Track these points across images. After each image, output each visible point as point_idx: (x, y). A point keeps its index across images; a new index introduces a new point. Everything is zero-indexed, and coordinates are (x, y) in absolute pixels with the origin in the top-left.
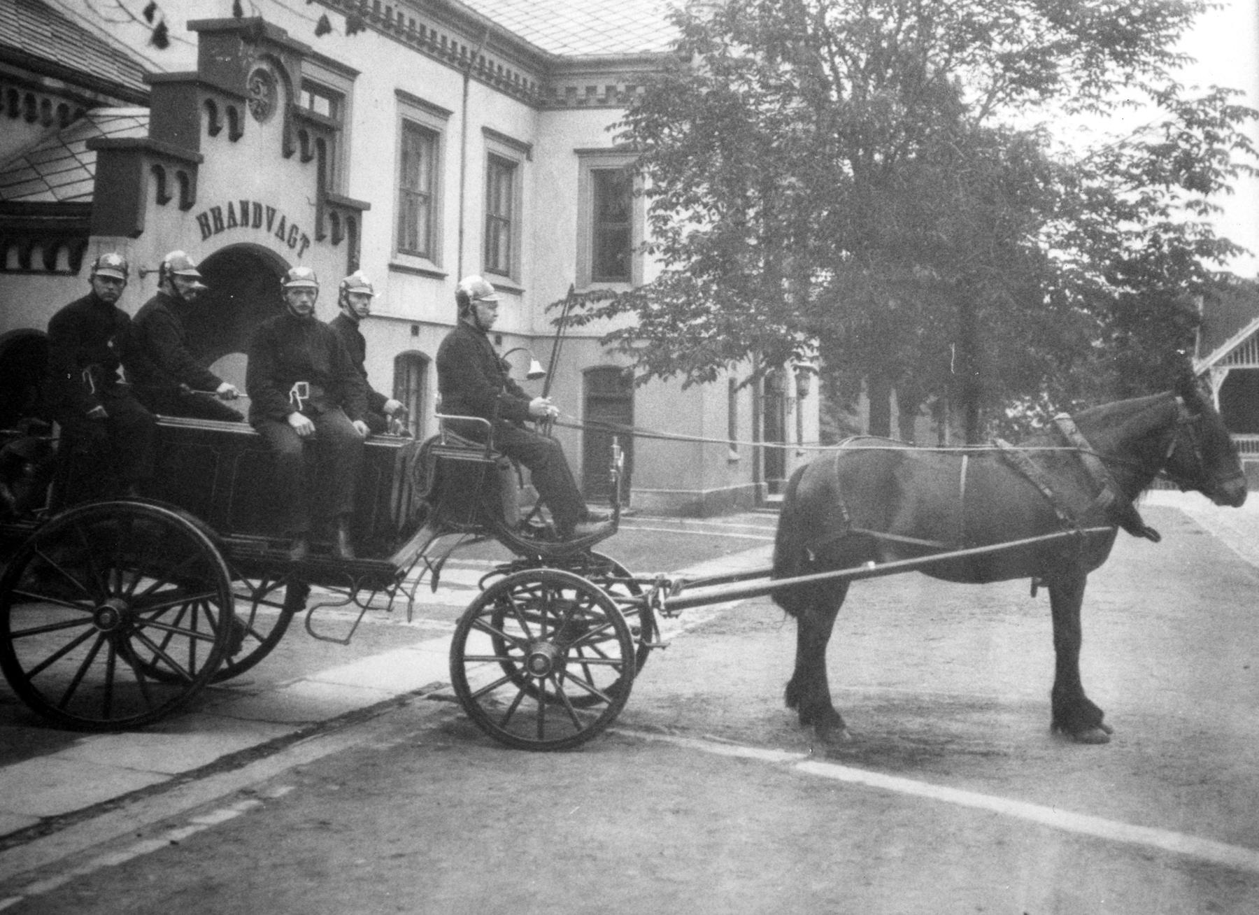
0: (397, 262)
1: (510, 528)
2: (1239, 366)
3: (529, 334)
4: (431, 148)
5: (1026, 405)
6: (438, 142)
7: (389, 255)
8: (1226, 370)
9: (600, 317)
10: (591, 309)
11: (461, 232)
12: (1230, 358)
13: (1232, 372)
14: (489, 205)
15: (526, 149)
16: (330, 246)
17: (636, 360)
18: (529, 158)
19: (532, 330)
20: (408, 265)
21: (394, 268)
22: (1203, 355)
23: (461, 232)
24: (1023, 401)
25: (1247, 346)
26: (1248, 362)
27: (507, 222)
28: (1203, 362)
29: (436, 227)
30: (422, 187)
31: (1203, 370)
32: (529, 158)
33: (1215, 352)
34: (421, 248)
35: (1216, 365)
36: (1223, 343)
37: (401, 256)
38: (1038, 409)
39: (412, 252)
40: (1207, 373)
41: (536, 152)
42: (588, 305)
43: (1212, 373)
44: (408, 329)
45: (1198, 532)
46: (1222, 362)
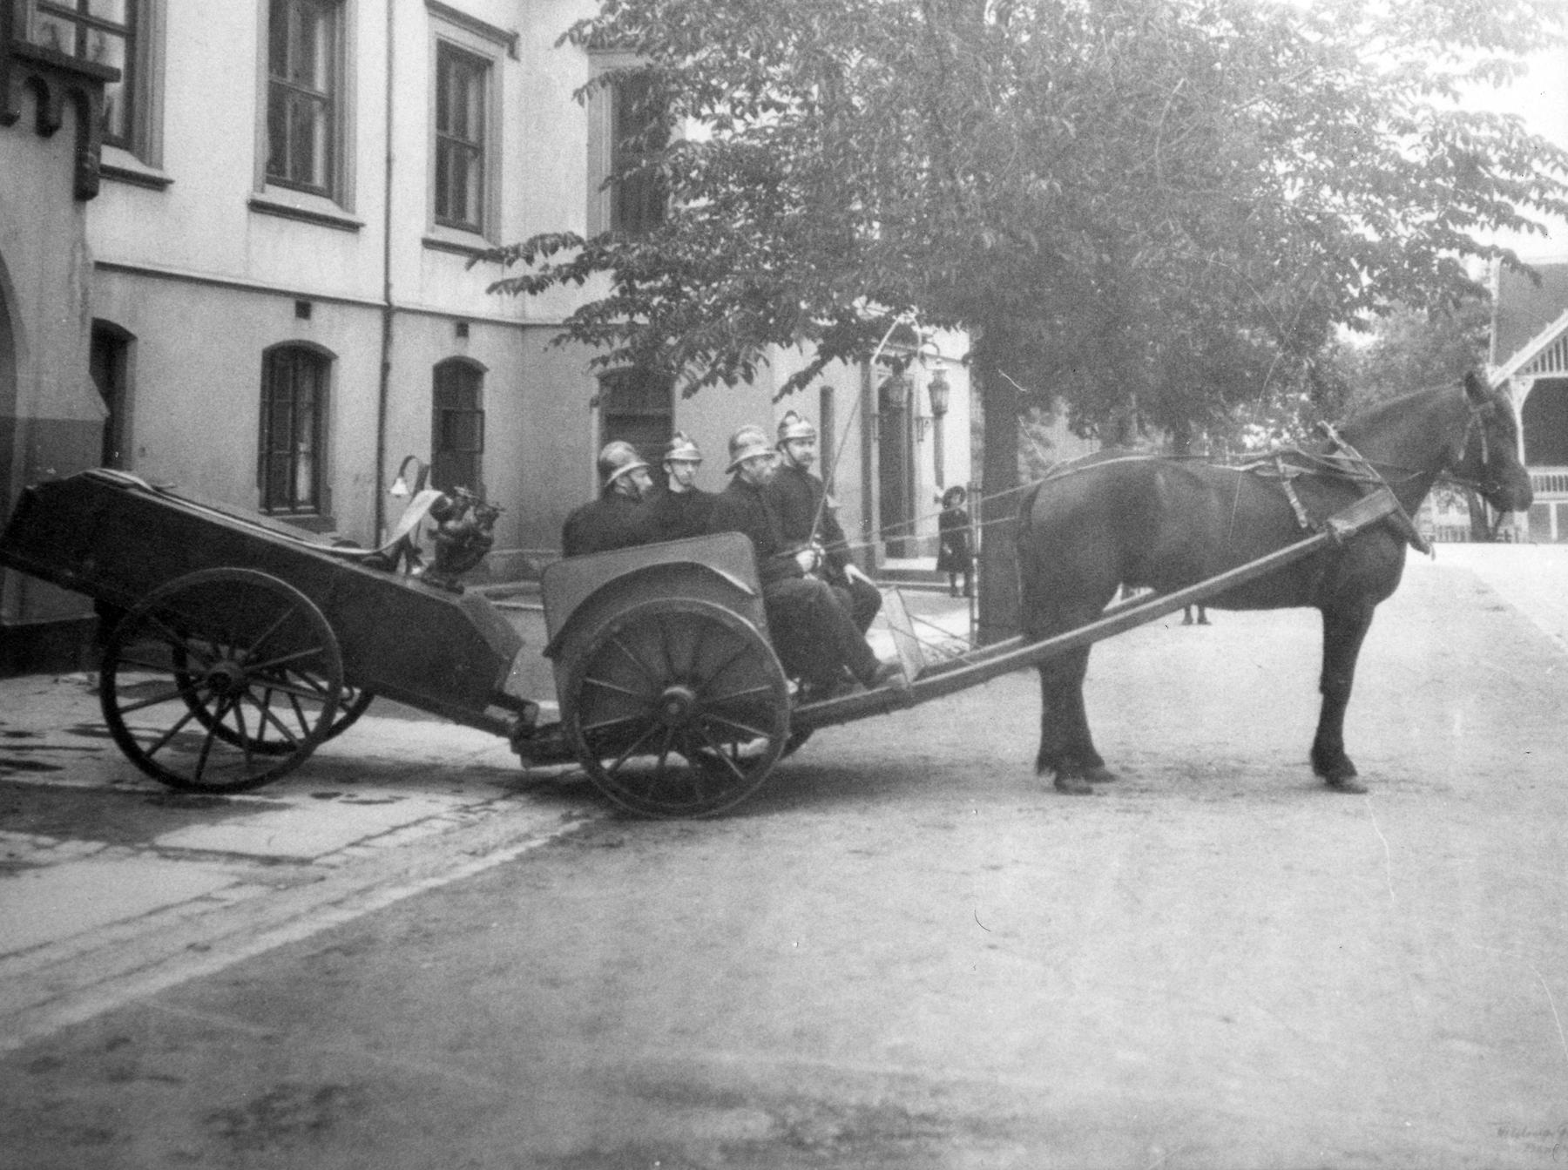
0: (433, 236)
1: (676, 477)
2: (1547, 375)
3: (518, 321)
4: (333, 23)
5: (1271, 430)
6: (343, 11)
7: (251, 188)
8: (1530, 380)
9: (564, 280)
10: (546, 267)
11: (389, 161)
12: (1536, 366)
13: (1539, 384)
14: (442, 123)
15: (509, 41)
16: (34, 139)
17: (811, 348)
18: (513, 54)
19: (524, 315)
20: (317, 210)
21: (257, 207)
22: (1500, 361)
23: (389, 161)
24: (1267, 426)
25: (1557, 346)
26: (1544, 369)
27: (478, 150)
28: (1500, 370)
29: (342, 141)
30: (320, 85)
31: (1501, 380)
32: (513, 54)
33: (1515, 355)
34: (319, 179)
35: (1517, 373)
36: (1525, 343)
37: (269, 188)
38: (1286, 436)
39: (301, 183)
40: (1506, 384)
41: (523, 48)
42: (539, 258)
43: (1513, 384)
44: (290, 306)
45: (1497, 608)
46: (1525, 369)
